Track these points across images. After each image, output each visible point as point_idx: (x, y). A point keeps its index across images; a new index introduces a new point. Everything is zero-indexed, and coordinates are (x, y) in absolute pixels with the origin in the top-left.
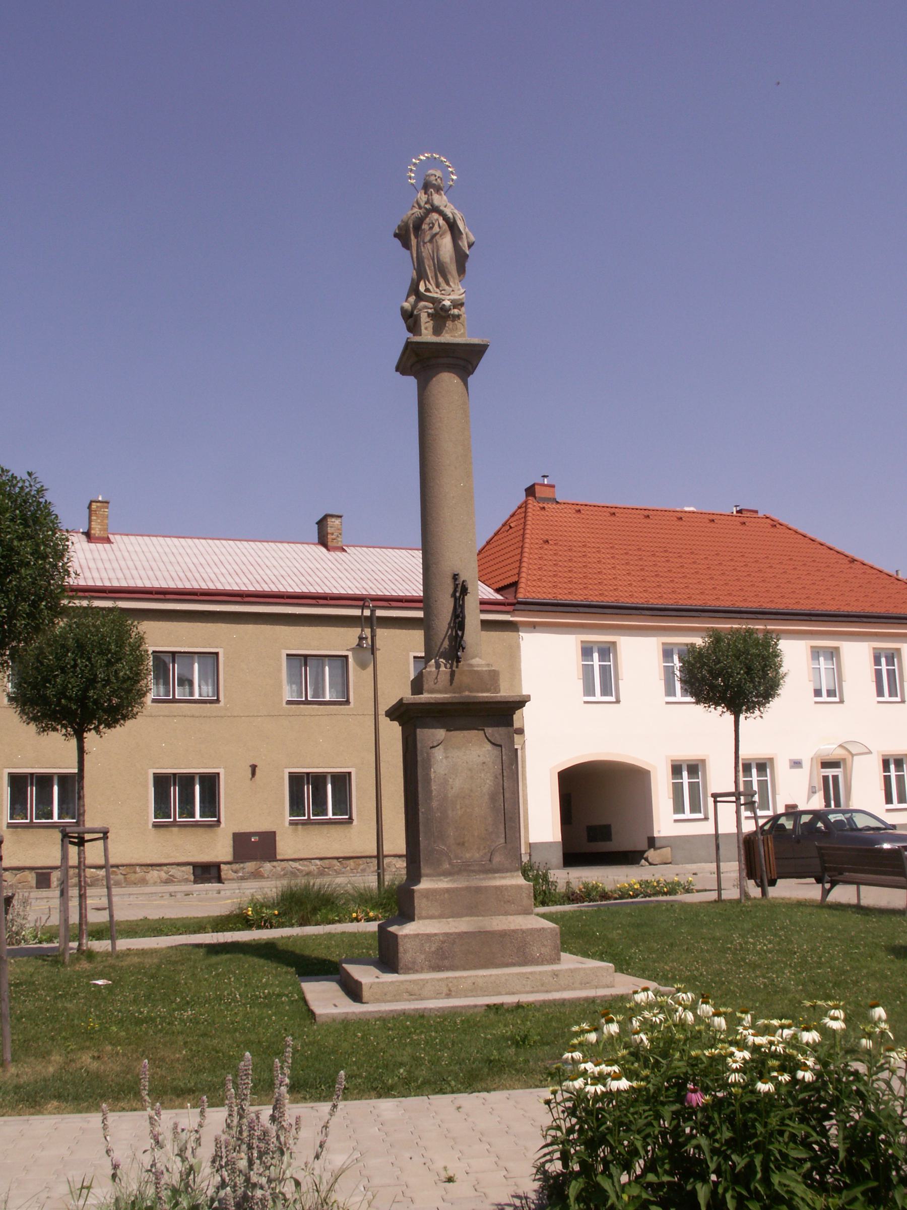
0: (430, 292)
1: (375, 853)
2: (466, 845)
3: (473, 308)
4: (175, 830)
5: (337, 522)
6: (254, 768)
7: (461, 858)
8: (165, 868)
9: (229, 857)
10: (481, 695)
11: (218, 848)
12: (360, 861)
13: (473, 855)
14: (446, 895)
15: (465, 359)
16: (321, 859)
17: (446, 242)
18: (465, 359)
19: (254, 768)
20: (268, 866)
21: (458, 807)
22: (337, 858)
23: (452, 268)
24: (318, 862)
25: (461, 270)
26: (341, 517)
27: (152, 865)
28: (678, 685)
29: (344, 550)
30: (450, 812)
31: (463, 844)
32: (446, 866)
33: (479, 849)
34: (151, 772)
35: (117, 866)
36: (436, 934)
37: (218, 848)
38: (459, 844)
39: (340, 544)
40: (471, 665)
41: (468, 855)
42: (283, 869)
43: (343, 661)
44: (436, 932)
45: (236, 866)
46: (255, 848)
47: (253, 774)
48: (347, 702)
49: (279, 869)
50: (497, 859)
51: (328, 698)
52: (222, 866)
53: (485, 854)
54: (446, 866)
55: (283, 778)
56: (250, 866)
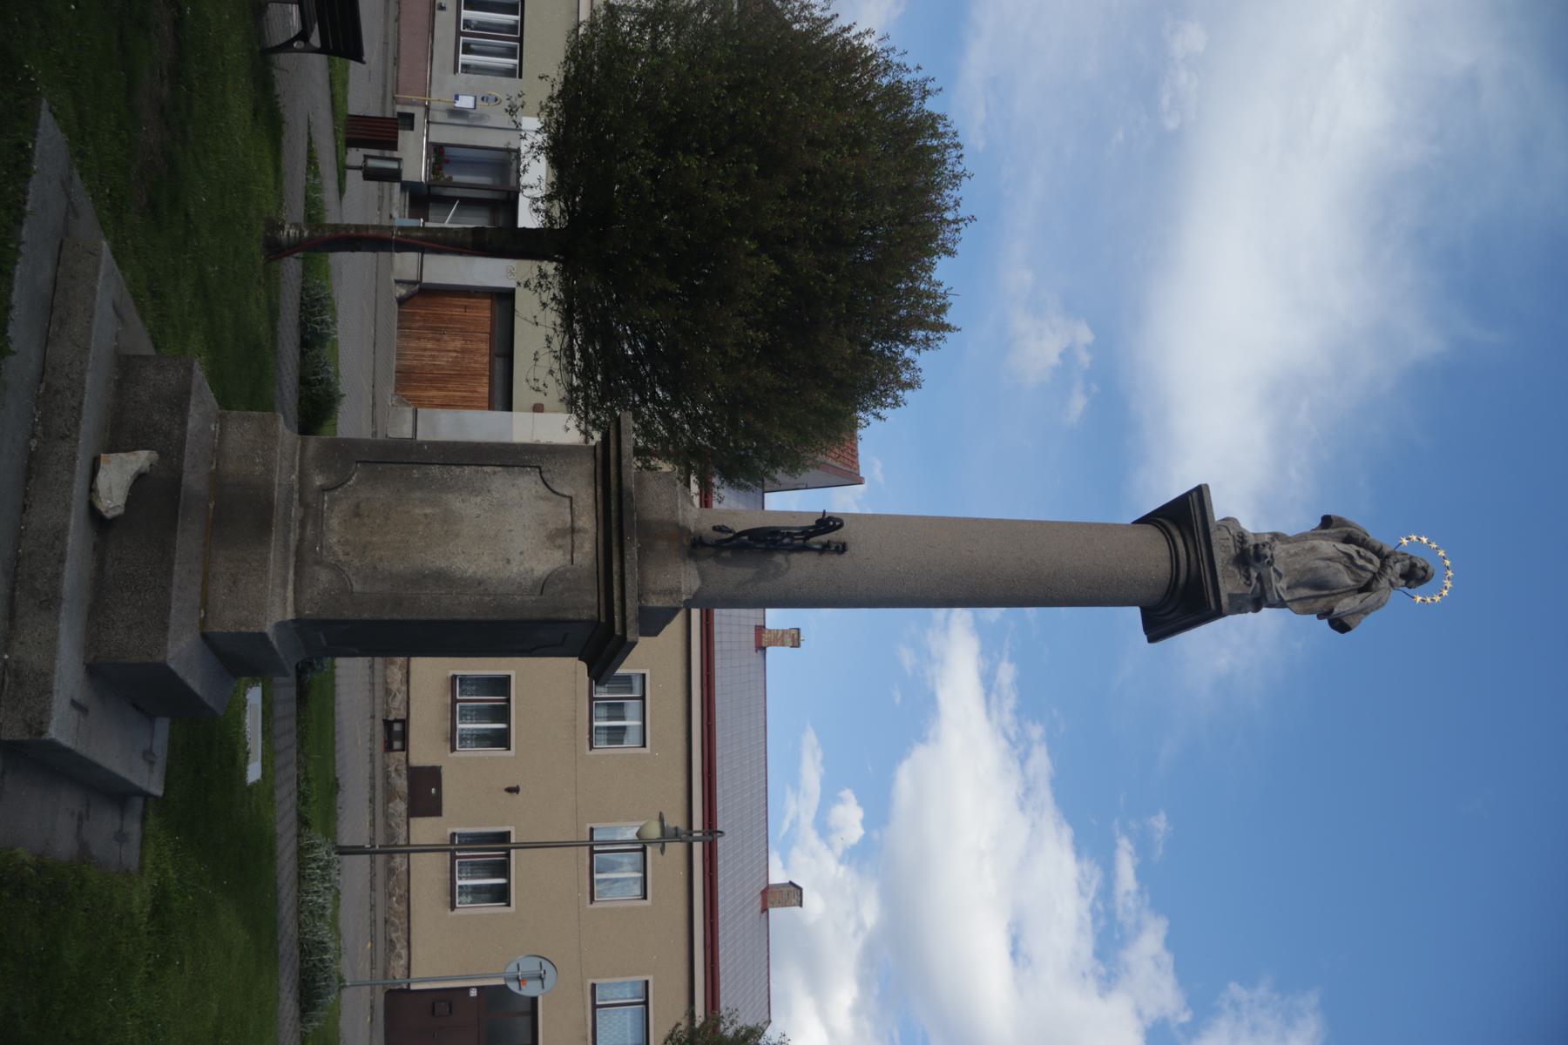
2: (356, 520)
4: (449, 700)
6: (513, 790)
7: (331, 509)
8: (404, 688)
11: (424, 749)
12: (404, 920)
20: (401, 806)
21: (428, 511)
24: (405, 867)
27: (408, 672)
28: (788, 503)
30: (418, 494)
31: (357, 515)
34: (512, 829)
36: (184, 423)
37: (424, 749)
38: (358, 506)
41: (334, 522)
44: (190, 425)
45: (403, 769)
46: (424, 791)
47: (510, 790)
53: (335, 554)
54: (319, 481)
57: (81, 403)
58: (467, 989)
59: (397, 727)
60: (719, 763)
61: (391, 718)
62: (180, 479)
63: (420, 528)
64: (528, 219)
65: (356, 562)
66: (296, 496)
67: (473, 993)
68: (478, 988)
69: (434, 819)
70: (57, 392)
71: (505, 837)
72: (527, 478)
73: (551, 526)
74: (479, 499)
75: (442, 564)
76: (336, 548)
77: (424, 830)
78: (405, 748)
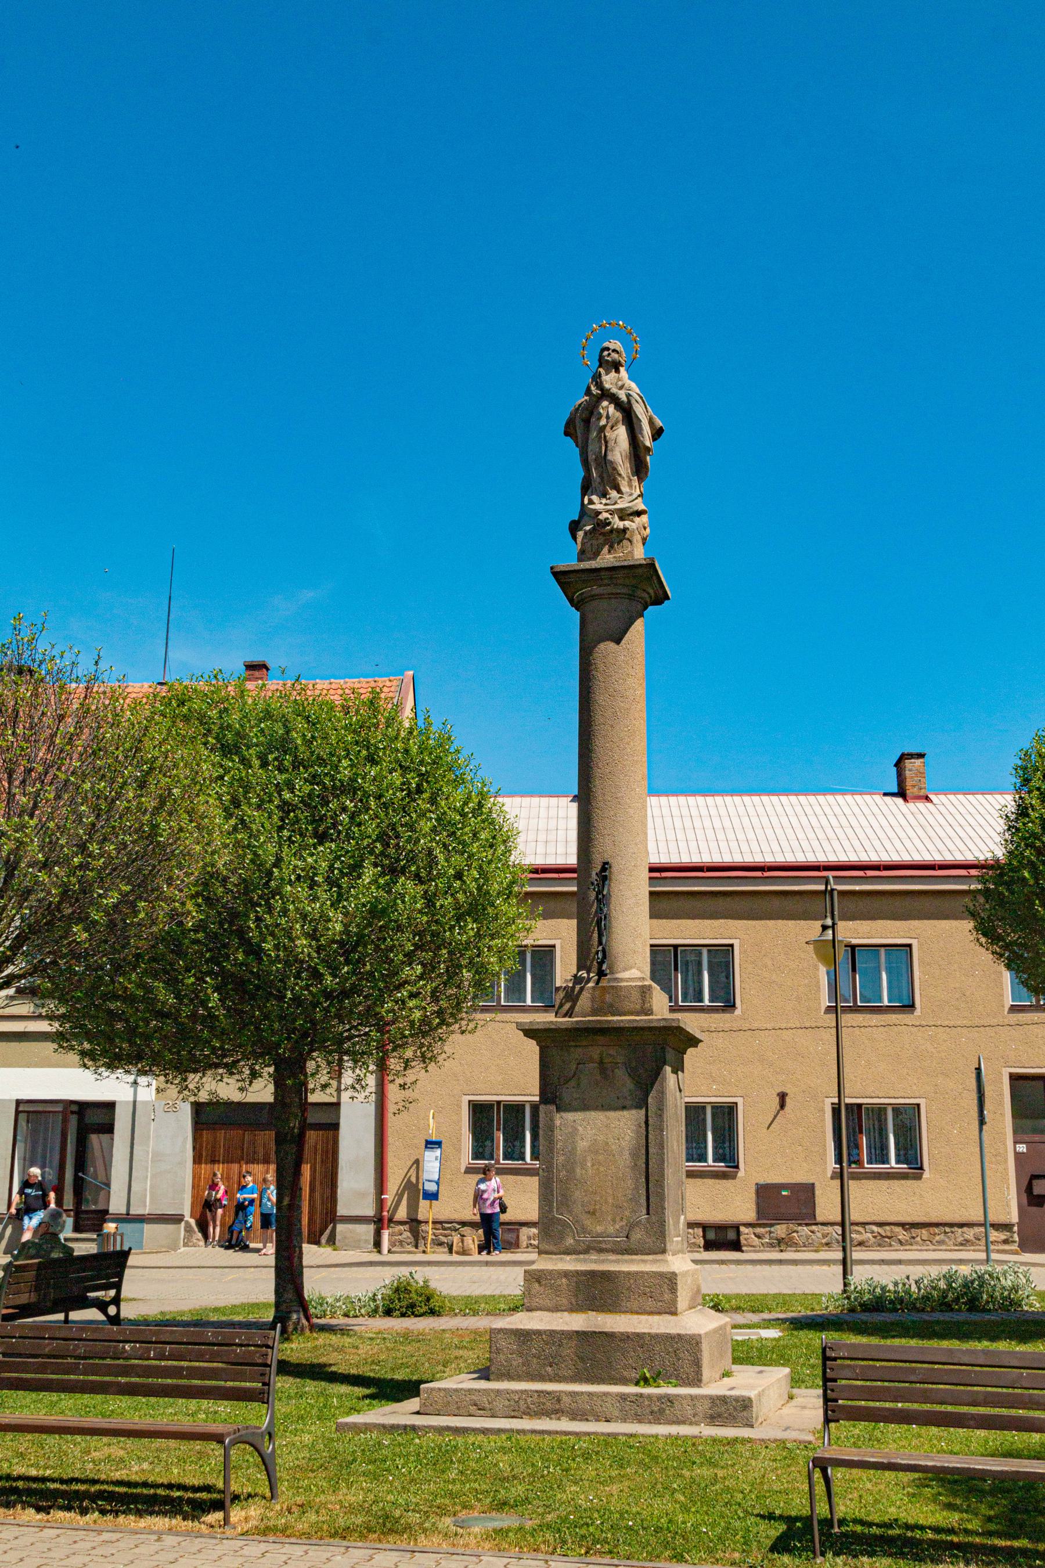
0: (593, 503)
1: (839, 1219)
3: (642, 520)
5: (918, 762)
6: (783, 1097)
9: (751, 1216)
10: (615, 1018)
13: (608, 1228)
14: (564, 1280)
15: (643, 587)
16: (880, 1224)
17: (620, 435)
18: (643, 587)
19: (783, 1097)
22: (902, 1225)
23: (624, 468)
24: (875, 1228)
25: (640, 469)
26: (921, 756)
29: (927, 798)
30: (578, 1170)
32: (570, 1241)
33: (614, 1220)
35: (864, 1224)
39: (922, 793)
40: (616, 979)
41: (599, 1229)
42: (824, 1236)
43: (903, 954)
46: (785, 1206)
47: (782, 1106)
48: (911, 1006)
49: (819, 1235)
50: (637, 1235)
51: (886, 1003)
52: (742, 1229)
55: (823, 1110)
56: (780, 1230)
57: (537, 1391)
58: (1018, 1155)
59: (711, 1235)
60: (839, 1195)
61: (701, 1242)
62: (577, 1332)
63: (602, 1169)
64: (263, 1091)
65: (627, 1213)
66: (582, 1256)
67: (1022, 1148)
68: (1015, 1143)
69: (818, 1192)
70: (528, 1407)
71: (836, 1111)
72: (564, 1095)
73: (599, 1078)
74: (580, 1128)
75: (626, 1155)
76: (617, 1227)
77: (827, 1207)
78: (736, 1227)
